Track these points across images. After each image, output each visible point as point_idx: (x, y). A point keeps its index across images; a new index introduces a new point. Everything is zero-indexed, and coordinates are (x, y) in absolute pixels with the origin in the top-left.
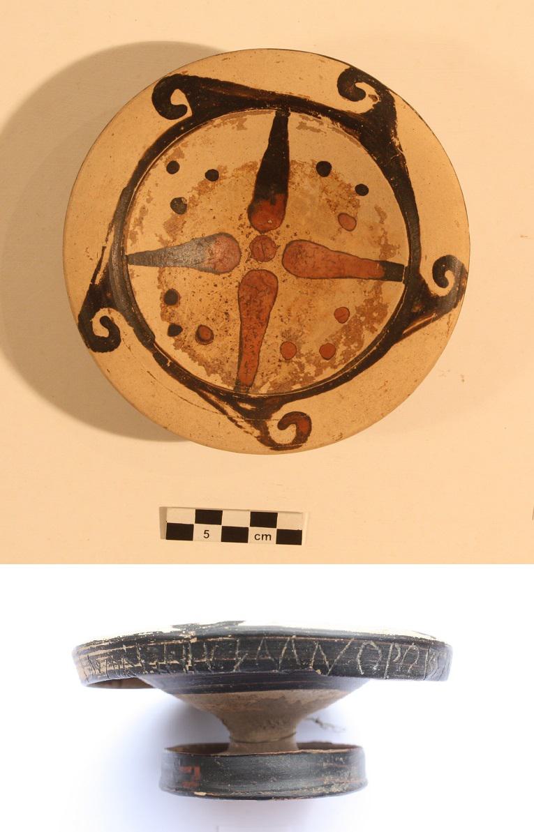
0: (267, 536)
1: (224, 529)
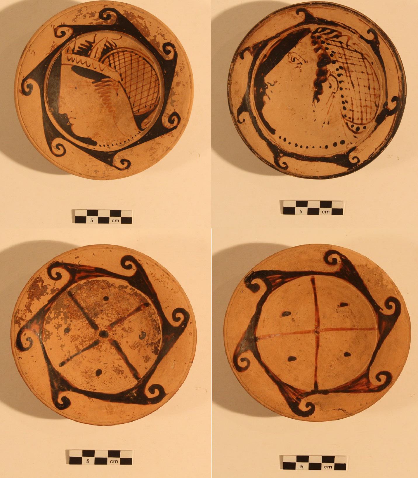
1: (99, 218)
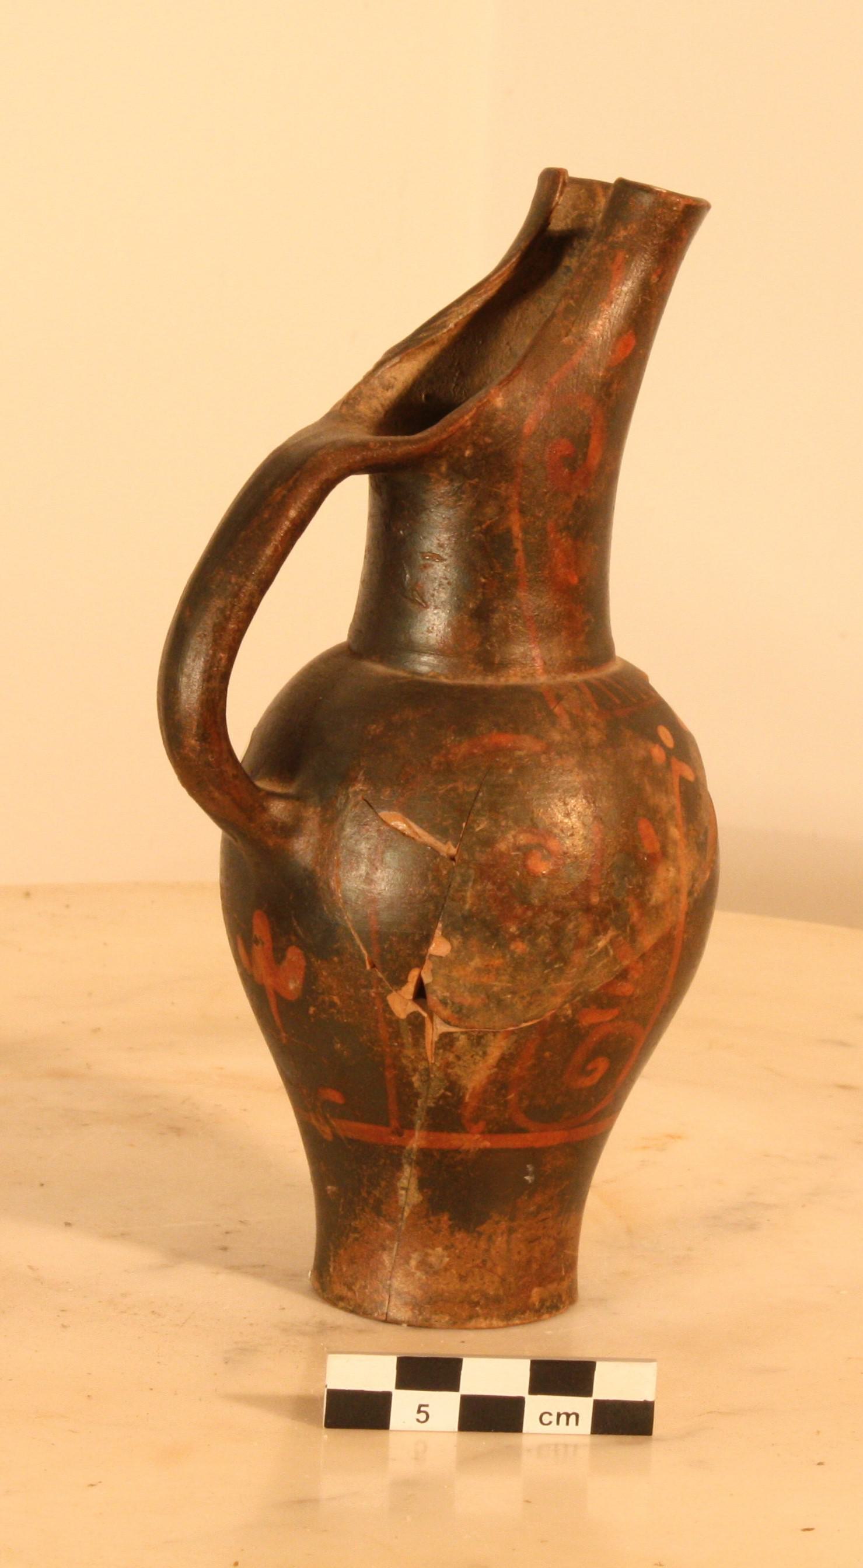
0: (568, 1415)
1: (468, 1402)
